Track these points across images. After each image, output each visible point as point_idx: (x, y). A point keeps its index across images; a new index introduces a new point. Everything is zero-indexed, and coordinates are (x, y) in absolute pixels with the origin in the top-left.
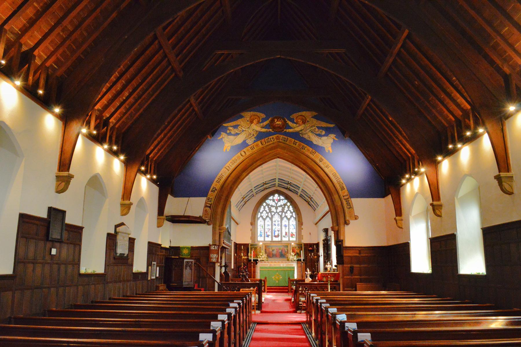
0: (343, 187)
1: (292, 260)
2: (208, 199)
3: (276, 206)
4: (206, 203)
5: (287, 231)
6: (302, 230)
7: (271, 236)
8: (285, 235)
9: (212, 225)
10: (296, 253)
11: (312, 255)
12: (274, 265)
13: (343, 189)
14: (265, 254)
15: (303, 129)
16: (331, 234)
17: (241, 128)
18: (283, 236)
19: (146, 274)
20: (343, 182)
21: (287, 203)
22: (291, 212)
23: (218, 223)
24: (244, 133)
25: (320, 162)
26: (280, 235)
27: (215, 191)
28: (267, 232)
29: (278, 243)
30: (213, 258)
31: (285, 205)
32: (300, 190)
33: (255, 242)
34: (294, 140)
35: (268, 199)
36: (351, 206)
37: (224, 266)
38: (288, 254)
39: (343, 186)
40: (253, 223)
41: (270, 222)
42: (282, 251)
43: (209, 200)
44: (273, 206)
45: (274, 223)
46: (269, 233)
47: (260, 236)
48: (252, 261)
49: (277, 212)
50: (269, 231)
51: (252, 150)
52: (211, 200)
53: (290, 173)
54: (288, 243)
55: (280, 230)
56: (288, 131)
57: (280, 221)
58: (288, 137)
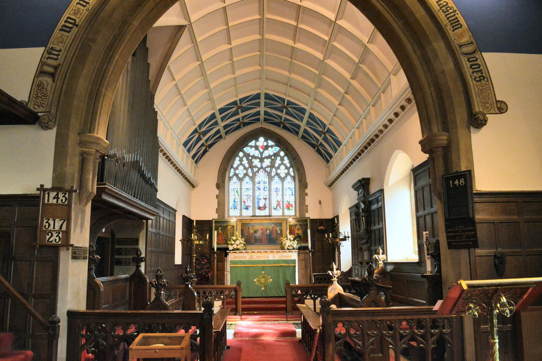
0: (458, 21)
1: (289, 248)
3: (260, 157)
4: (42, 63)
5: (280, 198)
6: (306, 197)
7: (252, 208)
8: (277, 207)
9: (55, 129)
10: (296, 235)
11: (331, 236)
12: (258, 257)
13: (456, 25)
14: (242, 238)
16: (383, 186)
18: (272, 208)
20: (455, 8)
21: (279, 152)
22: (286, 168)
23: (75, 124)
26: (267, 205)
27: (72, 28)
28: (246, 201)
29: (264, 218)
30: (50, 231)
31: (276, 155)
33: (224, 217)
35: (247, 145)
36: (484, 75)
38: (282, 238)
39: (457, 18)
40: (221, 185)
41: (251, 183)
42: (271, 232)
43: (51, 56)
44: (256, 158)
45: (257, 185)
46: (249, 203)
47: (233, 208)
48: (216, 251)
49: (262, 167)
50: (249, 200)
53: (286, 95)
54: (282, 219)
55: (268, 198)
57: (268, 183)
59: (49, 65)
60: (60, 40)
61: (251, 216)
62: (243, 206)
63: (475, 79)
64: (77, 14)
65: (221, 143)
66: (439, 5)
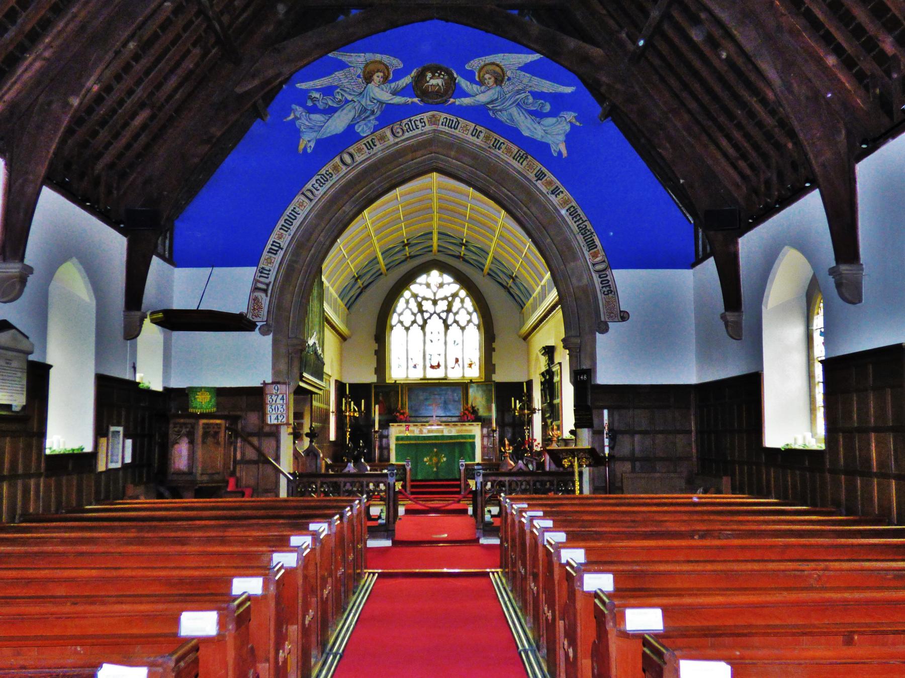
0: (594, 242)
4: (256, 281)
6: (493, 353)
15: (497, 99)
17: (342, 94)
19: (92, 457)
20: (593, 231)
23: (554, 529)
24: (348, 107)
25: (537, 180)
27: (277, 251)
31: (454, 295)
32: (490, 258)
34: (474, 125)
35: (415, 283)
36: (612, 289)
37: (307, 435)
43: (263, 275)
49: (435, 312)
51: (368, 149)
52: (268, 274)
56: (458, 102)
58: (459, 119)
59: (261, 283)
60: (269, 261)
61: (421, 379)
62: (411, 365)
63: (604, 293)
64: (281, 238)
65: (382, 279)
66: (579, 228)
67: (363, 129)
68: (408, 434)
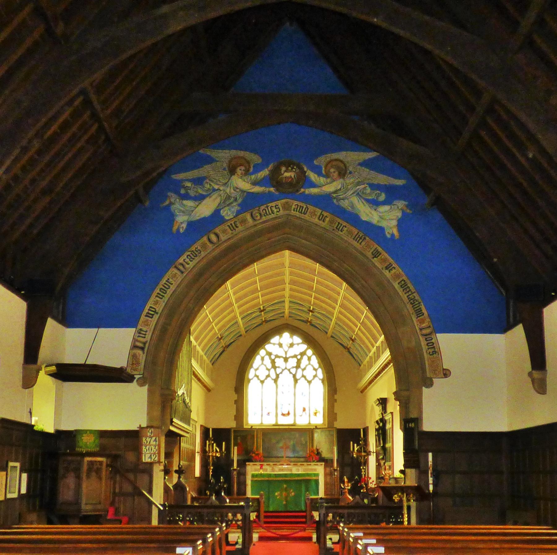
2: (140, 332)
4: (135, 340)
20: (420, 301)
27: (153, 315)
31: (303, 354)
36: (436, 350)
49: (286, 368)
61: (274, 425)
64: (156, 305)
67: (227, 213)
68: (261, 472)
